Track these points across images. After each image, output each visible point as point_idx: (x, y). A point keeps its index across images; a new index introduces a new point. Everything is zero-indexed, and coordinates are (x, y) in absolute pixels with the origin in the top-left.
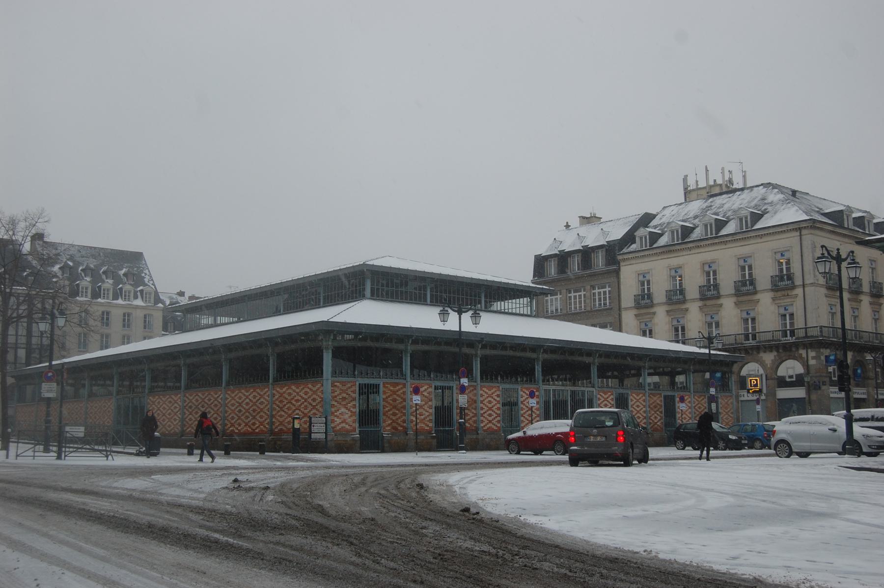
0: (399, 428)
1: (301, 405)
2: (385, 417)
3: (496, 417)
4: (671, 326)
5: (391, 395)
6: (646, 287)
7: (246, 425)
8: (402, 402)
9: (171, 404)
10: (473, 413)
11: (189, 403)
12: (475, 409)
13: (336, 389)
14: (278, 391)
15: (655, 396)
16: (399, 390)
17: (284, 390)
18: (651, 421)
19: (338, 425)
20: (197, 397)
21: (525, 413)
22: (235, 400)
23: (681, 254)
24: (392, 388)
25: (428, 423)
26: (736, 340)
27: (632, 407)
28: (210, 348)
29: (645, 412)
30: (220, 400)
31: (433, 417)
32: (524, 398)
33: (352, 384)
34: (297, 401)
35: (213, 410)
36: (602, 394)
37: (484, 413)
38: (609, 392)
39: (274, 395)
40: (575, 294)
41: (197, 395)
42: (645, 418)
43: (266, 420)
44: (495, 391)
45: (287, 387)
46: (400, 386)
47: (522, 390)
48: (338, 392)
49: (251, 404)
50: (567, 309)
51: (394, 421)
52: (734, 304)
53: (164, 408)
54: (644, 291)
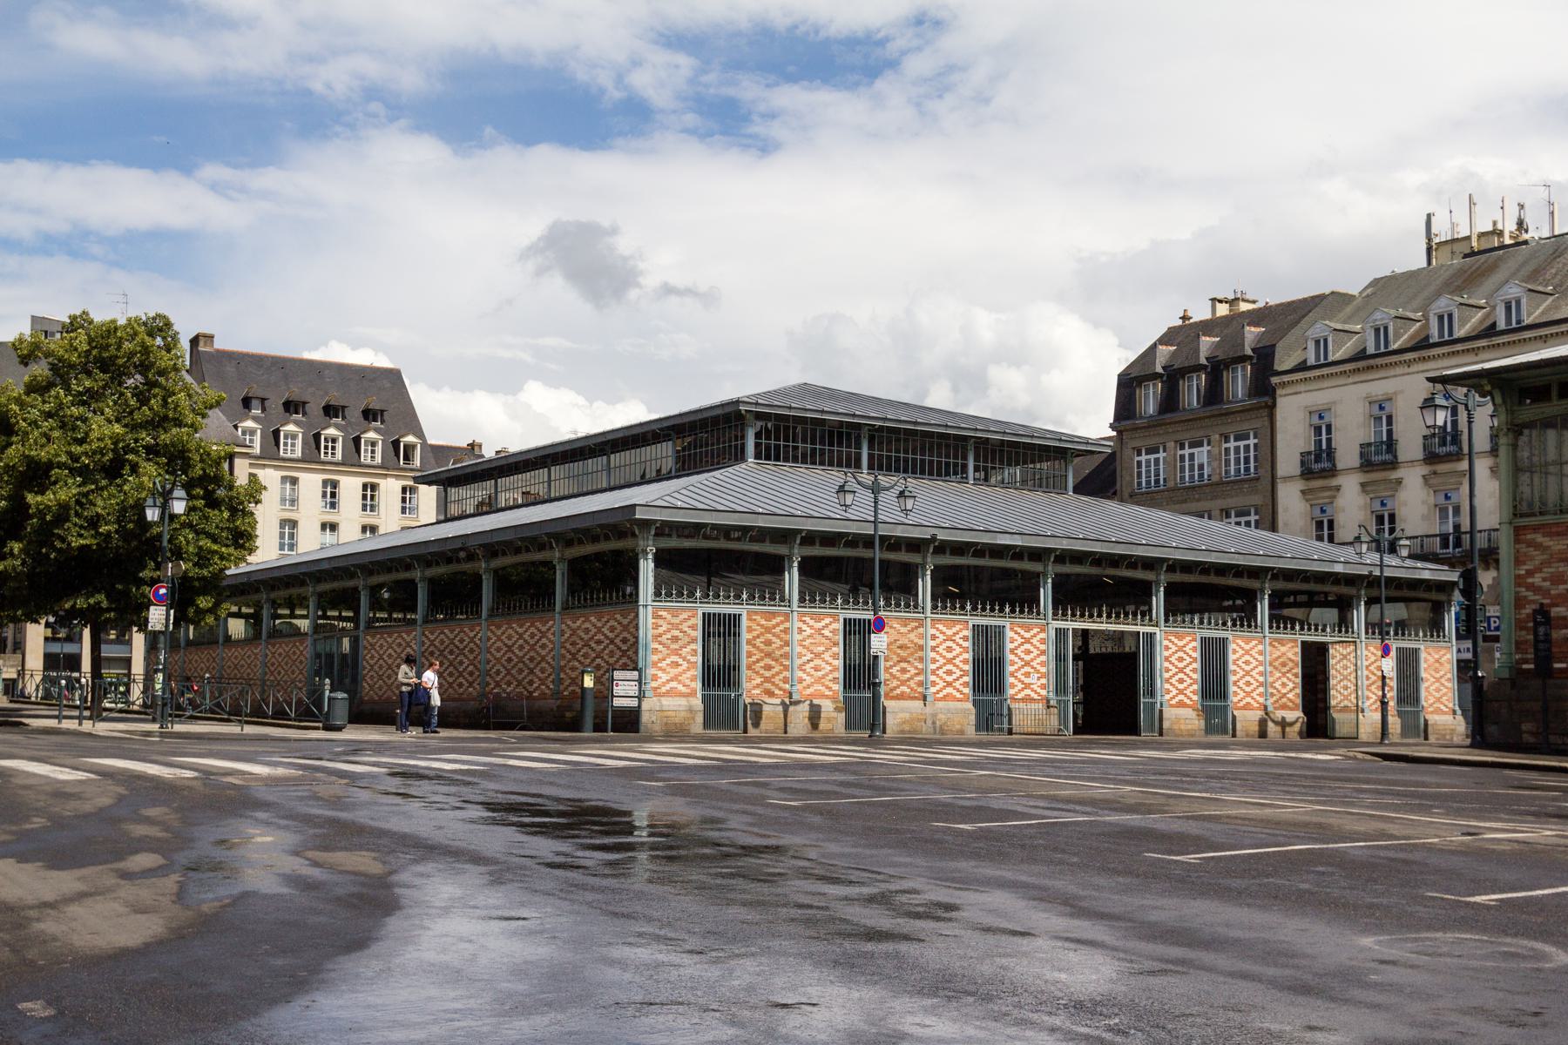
0: (777, 692)
1: (604, 649)
2: (750, 673)
3: (961, 676)
4: (1369, 512)
5: (762, 634)
6: (1324, 437)
7: (519, 683)
8: (781, 647)
9: (401, 649)
10: (916, 668)
11: (429, 647)
12: (921, 659)
13: (660, 622)
14: (568, 626)
15: (1283, 645)
16: (778, 625)
17: (578, 623)
18: (1275, 691)
19: (664, 684)
20: (442, 636)
21: (1017, 670)
22: (502, 641)
23: (1392, 372)
24: (763, 622)
25: (831, 684)
26: (1489, 540)
27: (1234, 663)
28: (461, 549)
29: (1261, 674)
30: (478, 642)
31: (840, 675)
32: (1016, 644)
33: (690, 614)
34: (599, 642)
35: (468, 658)
36: (1173, 638)
37: (938, 669)
38: (1189, 634)
39: (563, 633)
40: (1149, 457)
41: (442, 633)
42: (1261, 684)
43: (550, 675)
44: (961, 630)
45: (583, 619)
46: (779, 619)
47: (1012, 629)
48: (664, 628)
49: (527, 647)
50: (1175, 479)
51: (767, 680)
52: (1489, 471)
53: (390, 656)
54: (1321, 445)
